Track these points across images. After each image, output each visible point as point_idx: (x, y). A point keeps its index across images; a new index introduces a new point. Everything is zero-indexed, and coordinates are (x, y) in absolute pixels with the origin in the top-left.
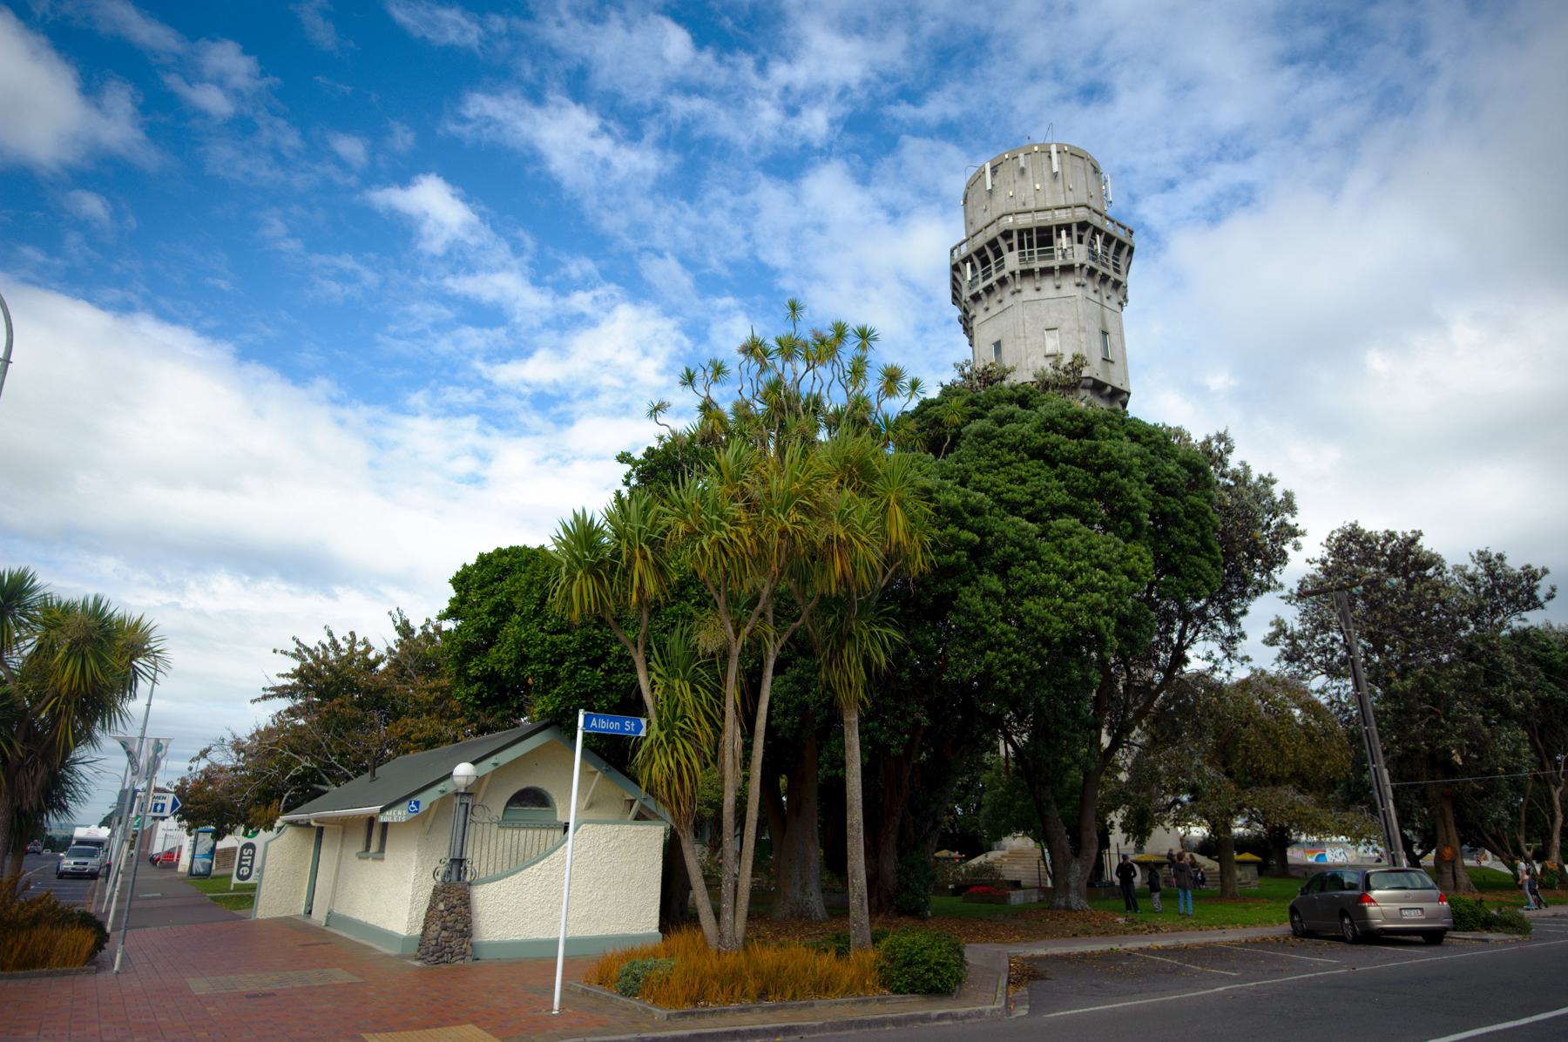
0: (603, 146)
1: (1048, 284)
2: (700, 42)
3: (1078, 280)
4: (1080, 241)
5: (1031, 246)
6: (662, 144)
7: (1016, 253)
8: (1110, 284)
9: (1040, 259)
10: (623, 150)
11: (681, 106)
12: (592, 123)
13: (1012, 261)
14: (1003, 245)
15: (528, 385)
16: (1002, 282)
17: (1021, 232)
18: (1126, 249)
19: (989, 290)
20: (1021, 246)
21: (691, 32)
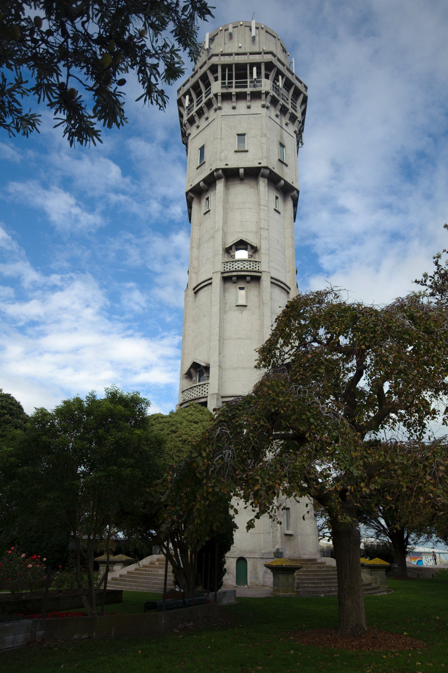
0: (76, 211)
1: (242, 106)
2: (124, 174)
3: (263, 103)
4: (267, 77)
5: (230, 78)
6: (104, 214)
7: (220, 82)
8: (288, 115)
9: (236, 87)
10: (85, 214)
11: (114, 198)
12: (72, 201)
13: (216, 87)
14: (211, 77)
15: (24, 315)
16: (209, 104)
17: (224, 66)
18: (302, 97)
19: (200, 113)
20: (223, 78)
21: (122, 169)
